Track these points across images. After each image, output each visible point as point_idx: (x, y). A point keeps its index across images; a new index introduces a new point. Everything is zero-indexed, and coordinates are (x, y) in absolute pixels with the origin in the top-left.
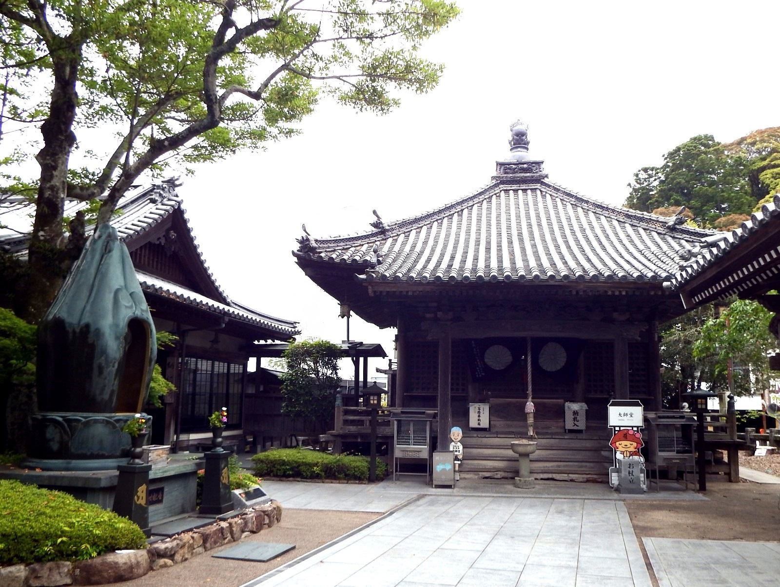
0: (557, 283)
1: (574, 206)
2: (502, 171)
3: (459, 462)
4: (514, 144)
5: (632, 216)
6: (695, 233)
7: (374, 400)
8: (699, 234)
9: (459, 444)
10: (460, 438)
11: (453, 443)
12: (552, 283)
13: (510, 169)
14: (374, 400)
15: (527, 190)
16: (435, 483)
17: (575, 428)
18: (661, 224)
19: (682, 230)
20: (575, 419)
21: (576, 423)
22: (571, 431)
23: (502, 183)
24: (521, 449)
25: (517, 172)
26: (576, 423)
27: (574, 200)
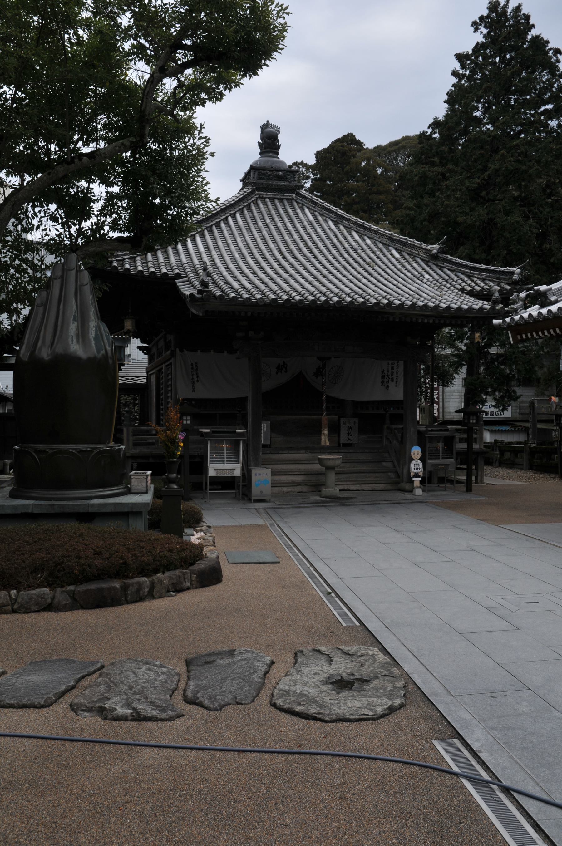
0: (391, 311)
1: (336, 224)
2: (256, 176)
3: (420, 479)
4: (265, 148)
5: (395, 240)
6: (457, 263)
7: (187, 420)
8: (460, 264)
9: (419, 461)
10: (419, 456)
11: (414, 462)
12: (376, 308)
13: (264, 175)
14: (187, 420)
15: (283, 199)
16: (253, 498)
17: (349, 442)
18: (424, 251)
19: (444, 259)
20: (349, 434)
21: (350, 437)
22: (345, 445)
23: (258, 189)
24: (330, 463)
25: (271, 179)
26: (350, 437)
27: (333, 216)
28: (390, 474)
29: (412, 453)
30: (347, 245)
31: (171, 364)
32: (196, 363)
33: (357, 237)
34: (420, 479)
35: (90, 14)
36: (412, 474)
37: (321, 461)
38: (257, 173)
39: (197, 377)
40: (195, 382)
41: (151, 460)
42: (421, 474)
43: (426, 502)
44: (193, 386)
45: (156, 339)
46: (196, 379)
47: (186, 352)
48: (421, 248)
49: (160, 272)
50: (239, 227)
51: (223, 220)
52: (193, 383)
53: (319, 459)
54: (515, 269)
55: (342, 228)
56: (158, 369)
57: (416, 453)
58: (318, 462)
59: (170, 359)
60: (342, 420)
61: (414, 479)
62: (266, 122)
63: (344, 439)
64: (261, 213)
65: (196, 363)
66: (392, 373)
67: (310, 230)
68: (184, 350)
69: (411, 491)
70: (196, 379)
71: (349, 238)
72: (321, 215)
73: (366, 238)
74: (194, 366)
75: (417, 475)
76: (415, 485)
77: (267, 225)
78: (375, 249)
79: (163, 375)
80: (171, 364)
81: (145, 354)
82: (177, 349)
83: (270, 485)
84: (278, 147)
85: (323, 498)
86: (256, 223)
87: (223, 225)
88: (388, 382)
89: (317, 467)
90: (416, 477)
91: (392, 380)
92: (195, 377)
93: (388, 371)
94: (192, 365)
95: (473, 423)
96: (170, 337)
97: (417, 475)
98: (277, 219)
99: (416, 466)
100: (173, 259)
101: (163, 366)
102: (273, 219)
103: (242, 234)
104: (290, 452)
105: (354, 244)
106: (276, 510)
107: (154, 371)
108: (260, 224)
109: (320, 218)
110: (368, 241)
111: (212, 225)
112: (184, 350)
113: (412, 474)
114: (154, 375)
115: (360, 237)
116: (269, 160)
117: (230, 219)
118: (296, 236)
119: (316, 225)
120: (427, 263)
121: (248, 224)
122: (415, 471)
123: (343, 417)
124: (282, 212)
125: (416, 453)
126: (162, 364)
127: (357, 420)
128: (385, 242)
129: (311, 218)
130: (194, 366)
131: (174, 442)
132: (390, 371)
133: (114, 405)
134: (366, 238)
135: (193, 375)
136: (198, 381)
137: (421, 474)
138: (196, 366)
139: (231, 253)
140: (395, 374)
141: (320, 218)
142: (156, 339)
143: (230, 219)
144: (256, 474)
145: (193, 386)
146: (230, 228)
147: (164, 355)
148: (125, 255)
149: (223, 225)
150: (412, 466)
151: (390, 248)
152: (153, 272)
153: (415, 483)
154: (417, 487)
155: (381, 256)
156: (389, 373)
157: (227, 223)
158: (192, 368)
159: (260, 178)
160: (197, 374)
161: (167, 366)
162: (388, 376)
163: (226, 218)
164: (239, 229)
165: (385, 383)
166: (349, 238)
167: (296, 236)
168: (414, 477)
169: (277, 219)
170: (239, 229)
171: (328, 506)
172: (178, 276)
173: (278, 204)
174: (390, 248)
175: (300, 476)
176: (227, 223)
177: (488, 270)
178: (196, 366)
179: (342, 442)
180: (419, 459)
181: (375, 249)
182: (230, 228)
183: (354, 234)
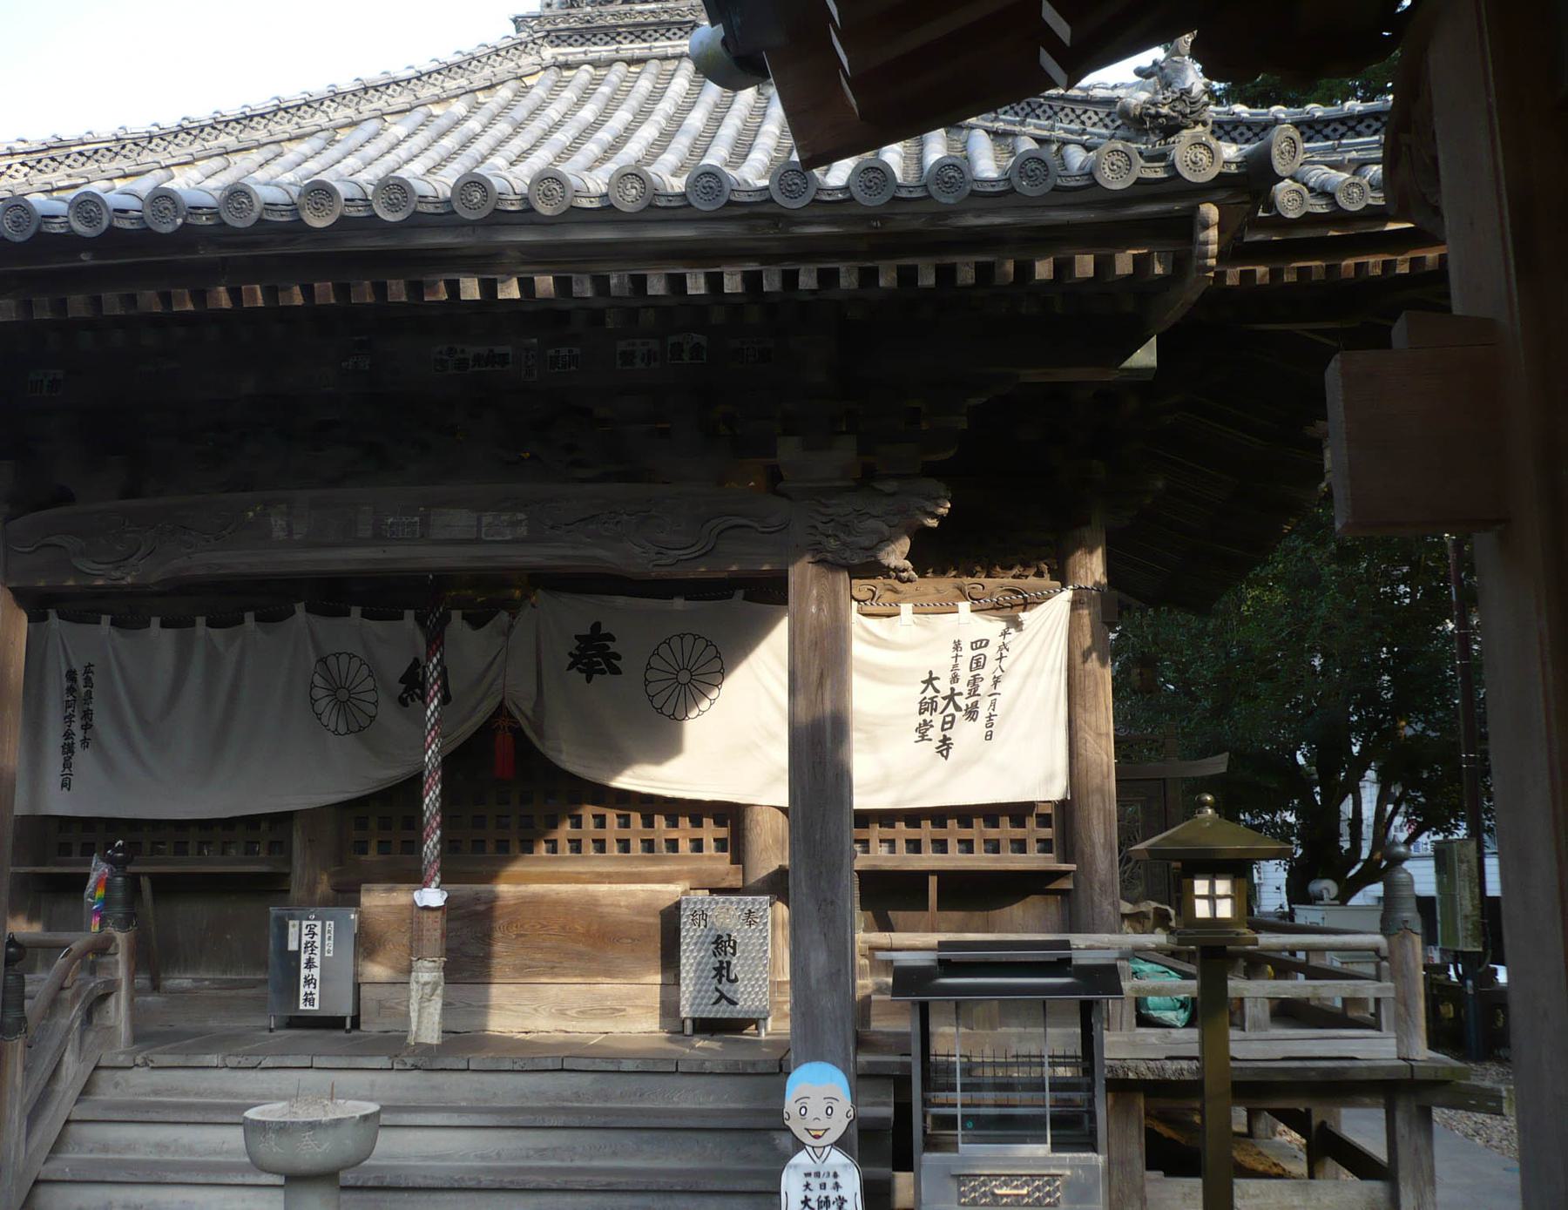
9: (837, 1158)
10: (838, 1125)
11: (801, 1158)
17: (723, 1011)
29: (790, 1106)
32: (88, 669)
35: (1423, 838)
39: (86, 727)
40: (78, 745)
46: (79, 735)
47: (54, 620)
57: (816, 1108)
65: (88, 669)
66: (974, 682)
68: (52, 613)
70: (79, 735)
88: (949, 723)
91: (972, 713)
92: (76, 727)
93: (955, 679)
94: (71, 675)
104: (318, 1062)
112: (52, 613)
125: (816, 1108)
132: (965, 674)
133: (977, 931)
138: (88, 681)
140: (984, 687)
145: (67, 764)
156: (961, 687)
158: (71, 690)
160: (87, 715)
162: (950, 698)
165: (935, 734)
178: (88, 681)
180: (840, 1144)
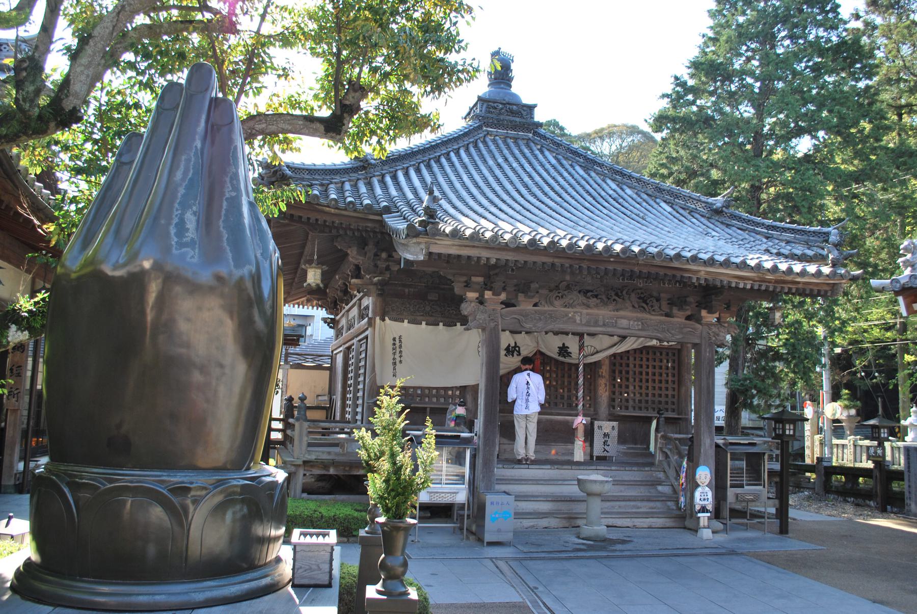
1: (586, 169)
4: (495, 79)
9: (707, 489)
10: (707, 481)
11: (699, 489)
16: (488, 538)
17: (605, 454)
18: (703, 205)
20: (605, 443)
21: (606, 447)
24: (596, 488)
26: (606, 447)
28: (669, 503)
29: (697, 476)
30: (603, 193)
31: (366, 337)
33: (614, 186)
34: (709, 514)
36: (698, 508)
37: (580, 482)
38: (485, 106)
41: (332, 471)
42: (710, 507)
43: (742, 554)
44: (394, 369)
45: (347, 308)
48: (700, 201)
49: (361, 204)
50: (464, 164)
51: (443, 154)
52: (395, 364)
53: (579, 480)
54: (830, 229)
55: (593, 174)
56: (347, 345)
57: (703, 477)
58: (576, 482)
59: (367, 329)
60: (596, 423)
61: (699, 515)
62: (497, 49)
63: (598, 450)
64: (490, 152)
67: (555, 174)
68: (387, 318)
69: (697, 531)
70: (398, 359)
71: (604, 185)
72: (566, 159)
73: (625, 187)
74: (397, 342)
75: (704, 509)
76: (701, 524)
77: (499, 165)
78: (639, 200)
79: (353, 353)
80: (366, 337)
81: (331, 327)
82: (378, 319)
83: (512, 516)
84: (510, 79)
85: (583, 539)
86: (485, 161)
87: (443, 160)
89: (573, 490)
90: (703, 512)
94: (394, 339)
95: (789, 435)
96: (368, 301)
97: (704, 509)
98: (511, 159)
99: (704, 496)
100: (378, 191)
101: (355, 341)
102: (506, 160)
103: (468, 172)
105: (611, 192)
106: (524, 563)
107: (341, 349)
108: (491, 162)
109: (564, 162)
110: (629, 191)
111: (430, 160)
113: (698, 508)
114: (342, 354)
115: (618, 185)
116: (499, 94)
117: (452, 154)
118: (537, 178)
119: (560, 168)
120: (708, 219)
121: (475, 161)
122: (701, 503)
123: (596, 419)
124: (517, 152)
125: (703, 477)
126: (353, 339)
127: (615, 424)
128: (650, 193)
129: (553, 161)
130: (397, 342)
131: (795, 366)
134: (625, 187)
135: (394, 354)
136: (401, 362)
137: (710, 507)
138: (400, 341)
139: (456, 191)
141: (564, 162)
142: (347, 308)
143: (452, 154)
144: (492, 503)
145: (394, 369)
146: (452, 165)
147: (356, 326)
148: (314, 179)
149: (443, 160)
150: (697, 494)
151: (658, 200)
152: (351, 202)
153: (701, 520)
154: (704, 528)
155: (648, 207)
157: (449, 159)
158: (394, 344)
159: (489, 112)
160: (400, 352)
161: (360, 341)
163: (448, 154)
164: (465, 167)
166: (604, 185)
167: (537, 178)
168: (699, 512)
169: (511, 159)
170: (465, 167)
171: (601, 557)
172: (387, 210)
173: (512, 145)
174: (658, 200)
175: (547, 503)
176: (449, 159)
177: (793, 230)
178: (400, 341)
179: (595, 454)
181: (639, 200)
182: (452, 165)
183: (609, 181)
